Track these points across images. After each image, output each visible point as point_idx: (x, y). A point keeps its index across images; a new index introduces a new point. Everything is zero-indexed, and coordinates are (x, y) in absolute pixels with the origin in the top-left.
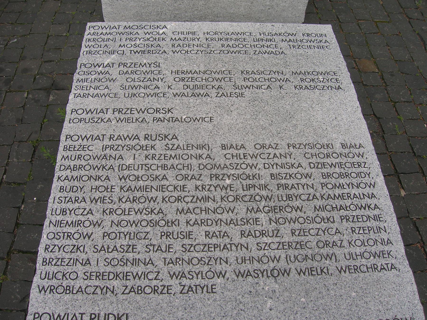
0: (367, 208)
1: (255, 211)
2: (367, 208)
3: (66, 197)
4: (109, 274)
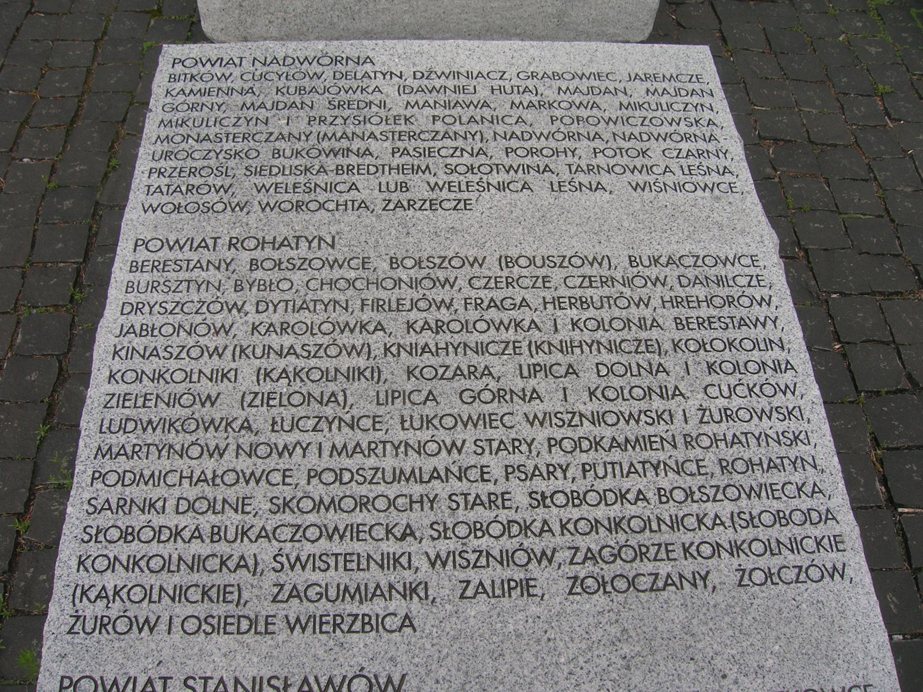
1: (350, 454)
2: (358, 329)
3: (188, 261)
4: (239, 620)
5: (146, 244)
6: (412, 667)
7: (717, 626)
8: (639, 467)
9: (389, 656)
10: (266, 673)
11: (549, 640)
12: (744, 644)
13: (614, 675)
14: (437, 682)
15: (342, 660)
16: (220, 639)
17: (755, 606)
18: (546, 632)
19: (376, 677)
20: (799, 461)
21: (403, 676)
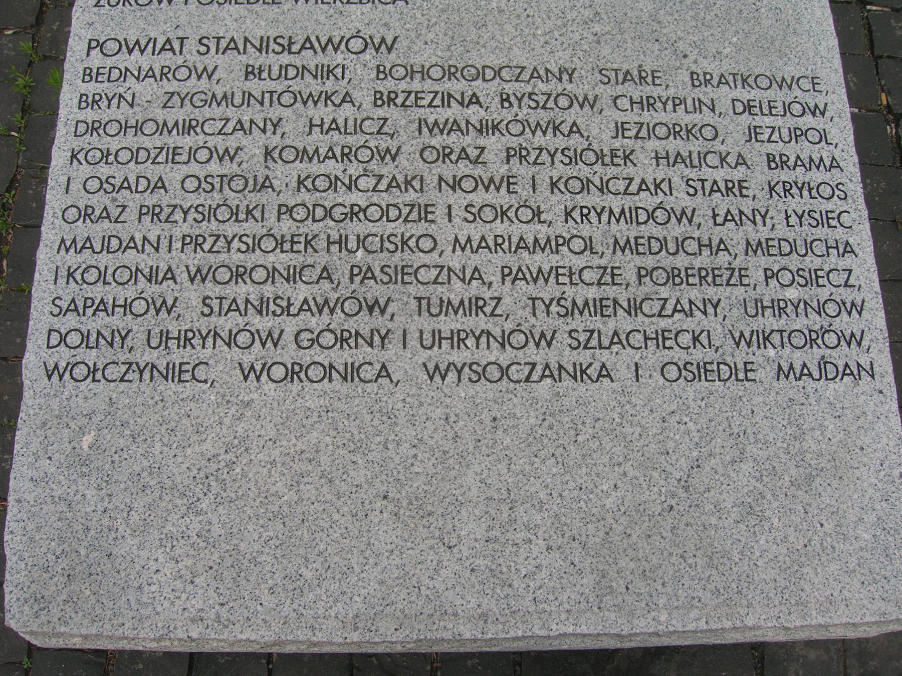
0: (550, 130)
5: (101, 46)
6: (404, 31)
7: (681, 18)
9: (384, 22)
10: (273, 34)
11: (528, 16)
12: (706, 34)
13: (586, 47)
14: (426, 43)
15: (341, 24)
16: (231, 8)
17: (717, 6)
18: (526, 10)
19: (371, 37)
20: (802, 305)
21: (396, 38)
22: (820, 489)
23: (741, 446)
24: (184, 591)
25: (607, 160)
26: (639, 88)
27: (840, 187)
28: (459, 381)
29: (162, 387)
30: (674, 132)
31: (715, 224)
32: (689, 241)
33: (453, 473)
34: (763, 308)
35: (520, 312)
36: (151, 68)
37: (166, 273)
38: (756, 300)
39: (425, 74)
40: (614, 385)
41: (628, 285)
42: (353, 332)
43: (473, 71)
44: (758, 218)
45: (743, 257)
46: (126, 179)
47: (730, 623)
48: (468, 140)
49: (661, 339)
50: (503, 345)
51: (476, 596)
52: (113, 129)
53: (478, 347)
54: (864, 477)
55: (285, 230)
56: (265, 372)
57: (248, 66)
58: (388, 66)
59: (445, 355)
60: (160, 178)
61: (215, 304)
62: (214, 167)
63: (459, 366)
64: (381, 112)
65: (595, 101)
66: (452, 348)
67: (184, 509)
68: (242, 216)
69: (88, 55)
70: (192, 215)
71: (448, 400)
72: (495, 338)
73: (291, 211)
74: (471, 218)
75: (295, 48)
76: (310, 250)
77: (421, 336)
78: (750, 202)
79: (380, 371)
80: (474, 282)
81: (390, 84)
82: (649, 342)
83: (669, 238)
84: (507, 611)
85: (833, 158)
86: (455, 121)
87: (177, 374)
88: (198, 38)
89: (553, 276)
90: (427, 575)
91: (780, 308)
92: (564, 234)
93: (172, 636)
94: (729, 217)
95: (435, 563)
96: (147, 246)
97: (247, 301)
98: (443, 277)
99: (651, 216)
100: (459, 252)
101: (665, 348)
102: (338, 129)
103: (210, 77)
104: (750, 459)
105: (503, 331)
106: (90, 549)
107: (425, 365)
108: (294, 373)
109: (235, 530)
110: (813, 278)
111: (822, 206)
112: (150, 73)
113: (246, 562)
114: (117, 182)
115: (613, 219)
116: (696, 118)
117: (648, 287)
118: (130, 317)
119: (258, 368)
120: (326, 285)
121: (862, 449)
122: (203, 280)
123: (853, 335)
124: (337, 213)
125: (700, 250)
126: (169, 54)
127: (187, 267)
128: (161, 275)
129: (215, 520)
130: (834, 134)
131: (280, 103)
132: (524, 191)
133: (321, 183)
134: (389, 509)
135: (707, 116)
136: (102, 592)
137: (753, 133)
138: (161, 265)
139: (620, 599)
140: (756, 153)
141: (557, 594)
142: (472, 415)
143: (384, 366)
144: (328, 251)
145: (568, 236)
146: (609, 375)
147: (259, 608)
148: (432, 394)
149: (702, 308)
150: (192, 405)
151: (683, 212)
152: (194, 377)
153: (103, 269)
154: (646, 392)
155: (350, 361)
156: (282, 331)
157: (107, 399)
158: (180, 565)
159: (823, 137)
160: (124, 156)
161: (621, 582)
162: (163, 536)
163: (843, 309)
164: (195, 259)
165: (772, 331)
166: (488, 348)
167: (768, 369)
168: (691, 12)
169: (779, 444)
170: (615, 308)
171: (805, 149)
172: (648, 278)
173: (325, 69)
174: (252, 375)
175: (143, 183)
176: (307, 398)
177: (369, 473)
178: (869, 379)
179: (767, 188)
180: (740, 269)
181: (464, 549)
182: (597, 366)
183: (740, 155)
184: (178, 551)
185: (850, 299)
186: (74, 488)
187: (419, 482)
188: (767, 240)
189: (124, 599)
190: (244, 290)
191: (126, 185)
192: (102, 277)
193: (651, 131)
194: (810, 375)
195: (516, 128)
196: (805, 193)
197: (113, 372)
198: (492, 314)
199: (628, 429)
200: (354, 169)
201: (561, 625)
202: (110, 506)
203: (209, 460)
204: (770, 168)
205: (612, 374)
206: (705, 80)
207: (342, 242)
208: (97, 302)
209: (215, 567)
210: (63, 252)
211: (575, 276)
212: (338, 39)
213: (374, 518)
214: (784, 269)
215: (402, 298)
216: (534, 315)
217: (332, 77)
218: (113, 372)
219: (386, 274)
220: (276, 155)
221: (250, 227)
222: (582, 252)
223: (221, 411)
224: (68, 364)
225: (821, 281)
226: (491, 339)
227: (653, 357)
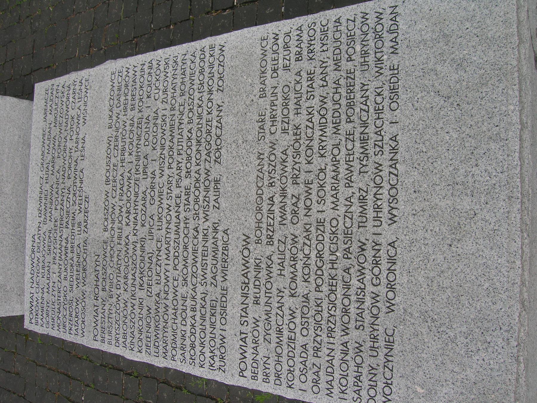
0: (285, 164)
5: (242, 371)
8: (180, 131)
10: (240, 291)
13: (249, 147)
19: (243, 246)
20: (363, 43)
21: (244, 235)
22: (450, 30)
23: (429, 71)
24: (494, 347)
25: (298, 137)
26: (266, 122)
27: (310, 26)
28: (397, 208)
29: (396, 351)
30: (286, 106)
31: (327, 85)
32: (334, 98)
33: (440, 212)
34: (365, 62)
35: (366, 179)
36: (253, 348)
37: (344, 346)
38: (361, 65)
39: (259, 222)
40: (400, 134)
41: (354, 128)
42: (373, 258)
43: (259, 199)
44: (324, 65)
45: (342, 72)
46: (301, 362)
47: (515, 73)
48: (289, 202)
49: (379, 111)
50: (381, 187)
51: (499, 202)
52: (279, 367)
53: (382, 199)
54: (444, 8)
55: (327, 289)
56: (391, 301)
57: (254, 303)
58: (256, 238)
59: (385, 215)
60: (302, 346)
61: (359, 323)
62: (298, 321)
63: (390, 208)
64: (276, 242)
65: (272, 143)
66: (381, 211)
67: (454, 345)
68: (320, 309)
69: (246, 377)
70: (318, 332)
71: (406, 214)
72: (377, 191)
73: (318, 286)
74: (323, 201)
75: (247, 281)
76: (336, 278)
77: (376, 226)
78: (317, 69)
79: (392, 246)
80: (352, 201)
81: (263, 238)
82: (380, 117)
83: (333, 108)
84: (507, 186)
85: (297, 29)
86: (280, 208)
87: (390, 344)
88: (241, 326)
89: (349, 163)
90: (488, 226)
91: (365, 54)
92: (331, 158)
93: (516, 355)
94: (324, 79)
95: (482, 222)
96: (331, 354)
97: (358, 308)
98: (349, 215)
99: (323, 116)
100: (338, 208)
101: (383, 109)
102: (282, 263)
103: (258, 321)
104: (435, 66)
105: (374, 187)
106: (472, 393)
107: (389, 225)
108: (391, 288)
109: (464, 320)
110: (351, 38)
111: (318, 35)
112: (255, 348)
113: (480, 316)
114: (302, 367)
115: (324, 135)
116: (279, 95)
117: (355, 118)
118: (363, 365)
119: (388, 304)
120: (352, 271)
121: (431, 10)
122: (348, 328)
123: (377, 17)
124: (319, 264)
125: (339, 93)
126: (247, 339)
127: (342, 336)
128: (345, 349)
129: (459, 330)
130: (286, 29)
131: (271, 289)
132: (312, 176)
133: (306, 271)
134: (456, 244)
135: (279, 90)
136: (493, 389)
137: (286, 68)
138: (340, 348)
139: (502, 130)
140: (295, 66)
141: (499, 162)
142: (413, 202)
143: (389, 245)
144: (336, 269)
145: (332, 156)
146: (395, 137)
147: (503, 310)
148: (402, 221)
149: (365, 92)
150: (404, 337)
151: (321, 101)
152: (392, 336)
153: (341, 376)
154: (403, 118)
155: (386, 261)
156: (372, 292)
157: (401, 379)
158: (481, 348)
159: (287, 34)
160: (291, 363)
161: (494, 129)
162: (466, 356)
163: (365, 23)
164: (338, 332)
165: (375, 57)
166: (382, 194)
167: (393, 58)
168: (233, 98)
169: (428, 52)
170: (364, 134)
171: (293, 43)
172: (351, 118)
173: (256, 267)
174: (392, 307)
175: (303, 355)
176: (403, 282)
177: (439, 253)
178: (397, 8)
179: (310, 61)
180: (347, 73)
181: (476, 207)
182: (391, 142)
183: (296, 74)
184: (474, 349)
185: (360, 19)
186: (442, 398)
187: (444, 229)
188: (334, 61)
189: (497, 378)
190: (353, 309)
191: (304, 363)
192: (345, 377)
193: (286, 116)
194: (396, 38)
195: (284, 180)
196: (313, 42)
197: (388, 375)
198: (367, 192)
199: (421, 127)
200: (300, 255)
201: (515, 159)
202: (451, 381)
203: (430, 331)
204: (302, 60)
205: (394, 135)
206: (263, 91)
207: (333, 262)
208: (356, 380)
209: (482, 331)
210: (332, 395)
211: (350, 153)
212: (243, 261)
213: (460, 251)
214: (347, 52)
215: (358, 235)
216: (367, 172)
217: (260, 265)
218: (388, 375)
219: (347, 242)
220: (293, 292)
221: (325, 305)
222: (339, 149)
223: (408, 323)
224: (383, 396)
225: (352, 34)
226: (378, 193)
227: (387, 115)
